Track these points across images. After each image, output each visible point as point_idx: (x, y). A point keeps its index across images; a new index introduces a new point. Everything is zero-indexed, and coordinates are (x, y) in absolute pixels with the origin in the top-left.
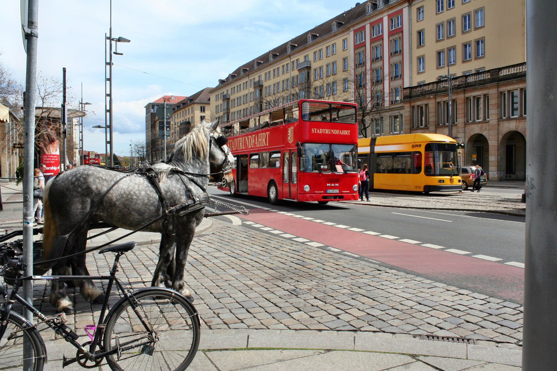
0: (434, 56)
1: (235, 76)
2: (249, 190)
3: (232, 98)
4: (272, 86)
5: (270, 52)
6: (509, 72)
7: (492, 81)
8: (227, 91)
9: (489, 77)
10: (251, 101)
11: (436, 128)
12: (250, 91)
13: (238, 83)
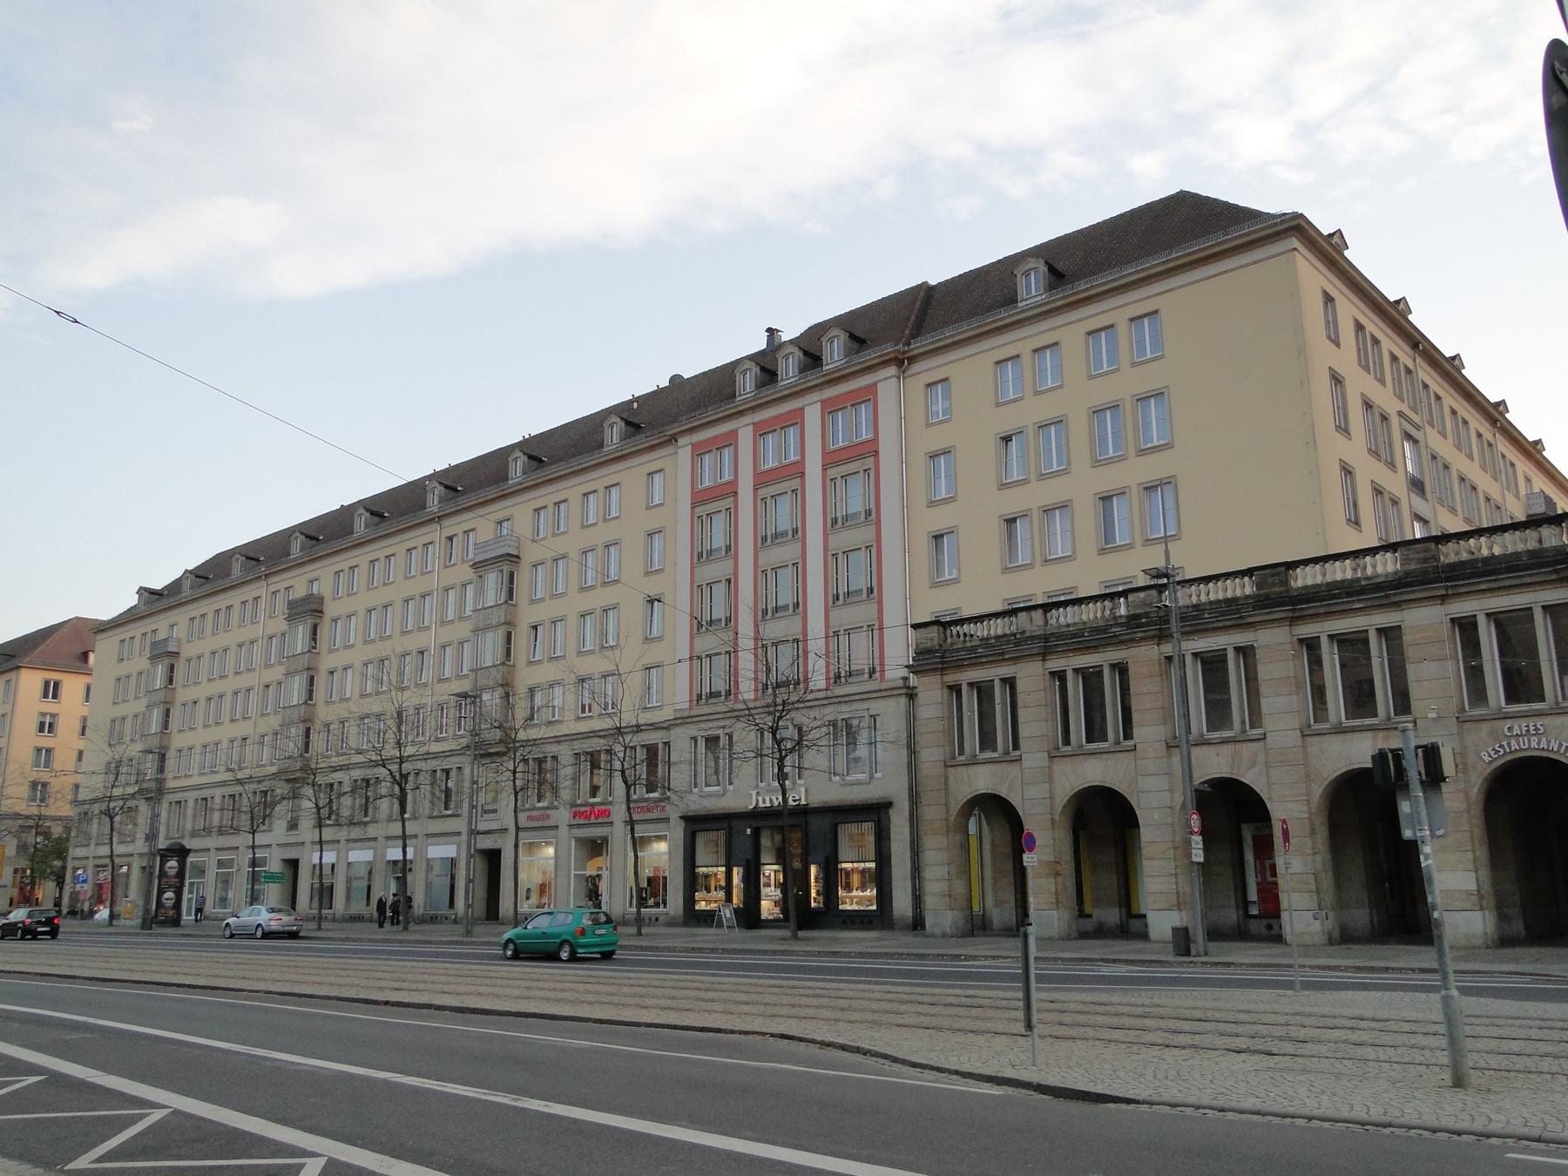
1: (211, 577)
2: (1169, 820)
3: (187, 651)
5: (436, 476)
6: (1324, 575)
7: (1262, 602)
9: (1248, 591)
10: (267, 666)
11: (1051, 757)
13: (221, 602)
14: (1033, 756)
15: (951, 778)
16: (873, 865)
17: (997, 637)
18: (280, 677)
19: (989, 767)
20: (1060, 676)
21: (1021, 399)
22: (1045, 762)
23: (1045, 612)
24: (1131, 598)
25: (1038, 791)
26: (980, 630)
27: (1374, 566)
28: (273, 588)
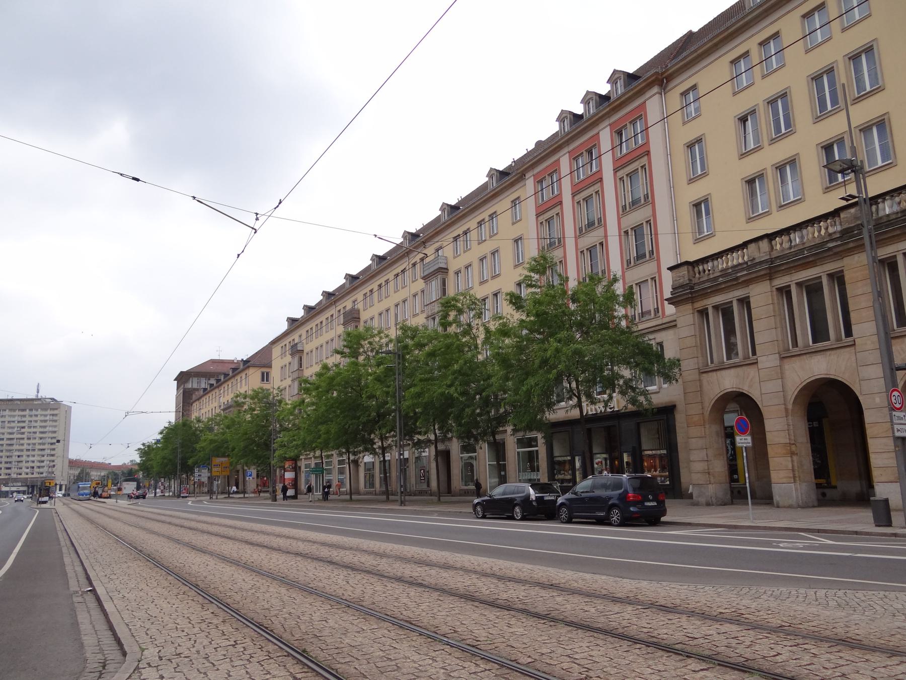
0: (739, 190)
3: (307, 348)
4: (376, 317)
8: (300, 336)
11: (783, 359)
12: (338, 333)
14: (767, 360)
15: (705, 383)
16: (665, 452)
17: (734, 267)
18: (290, 383)
19: (733, 371)
20: (785, 291)
21: (753, 84)
22: (777, 363)
23: (789, 234)
24: (842, 215)
25: (773, 386)
26: (721, 264)
27: (781, 244)
28: (338, 309)
